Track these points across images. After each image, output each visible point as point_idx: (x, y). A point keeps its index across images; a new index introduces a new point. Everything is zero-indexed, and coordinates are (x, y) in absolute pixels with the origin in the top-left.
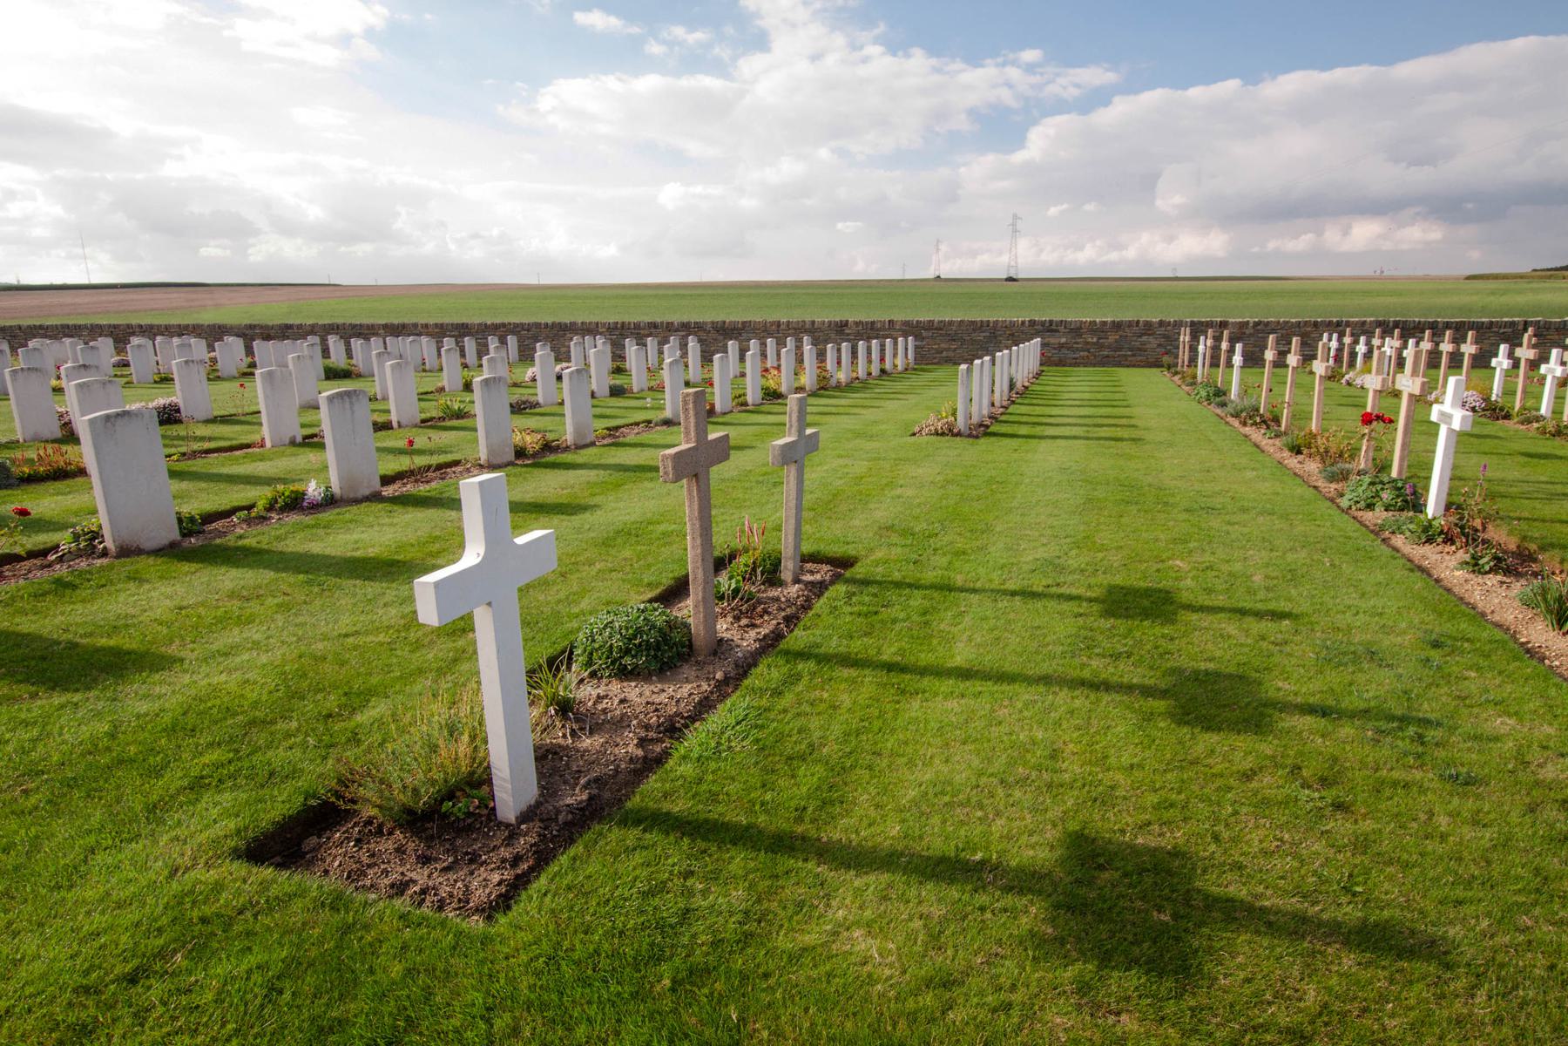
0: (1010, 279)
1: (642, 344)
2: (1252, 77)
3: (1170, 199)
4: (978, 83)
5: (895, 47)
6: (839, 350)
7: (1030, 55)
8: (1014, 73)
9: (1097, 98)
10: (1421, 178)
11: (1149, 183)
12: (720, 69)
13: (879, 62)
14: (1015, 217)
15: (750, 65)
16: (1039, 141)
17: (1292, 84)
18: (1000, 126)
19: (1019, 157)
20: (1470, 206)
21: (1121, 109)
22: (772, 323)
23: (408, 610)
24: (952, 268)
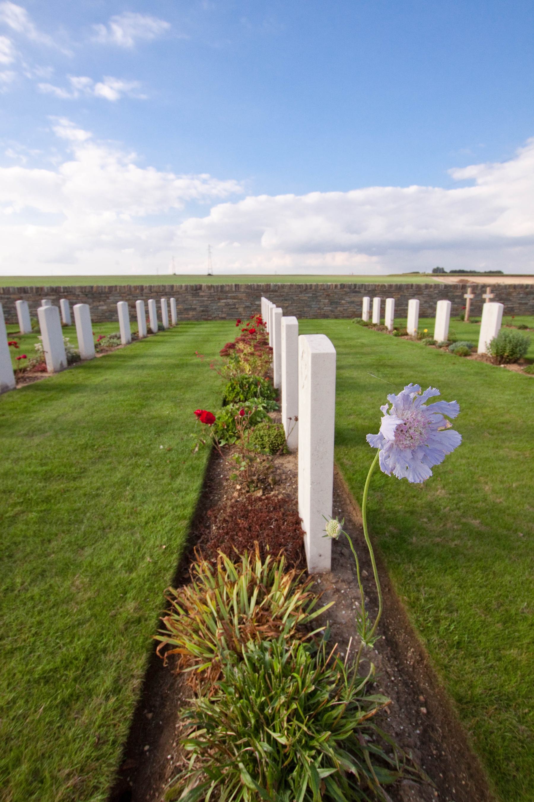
0: (209, 275)
1: (56, 303)
2: (273, 193)
3: (267, 240)
4: (181, 185)
5: (141, 165)
6: (146, 305)
7: (205, 176)
8: (197, 183)
9: (234, 198)
10: (354, 238)
11: (257, 236)
12: (50, 167)
13: (135, 174)
14: (209, 246)
15: (68, 168)
16: (217, 214)
17: (313, 197)
18: (197, 207)
19: (206, 220)
20: (374, 249)
21: (249, 203)
22: (136, 288)
23: (398, 320)
24: (181, 271)
